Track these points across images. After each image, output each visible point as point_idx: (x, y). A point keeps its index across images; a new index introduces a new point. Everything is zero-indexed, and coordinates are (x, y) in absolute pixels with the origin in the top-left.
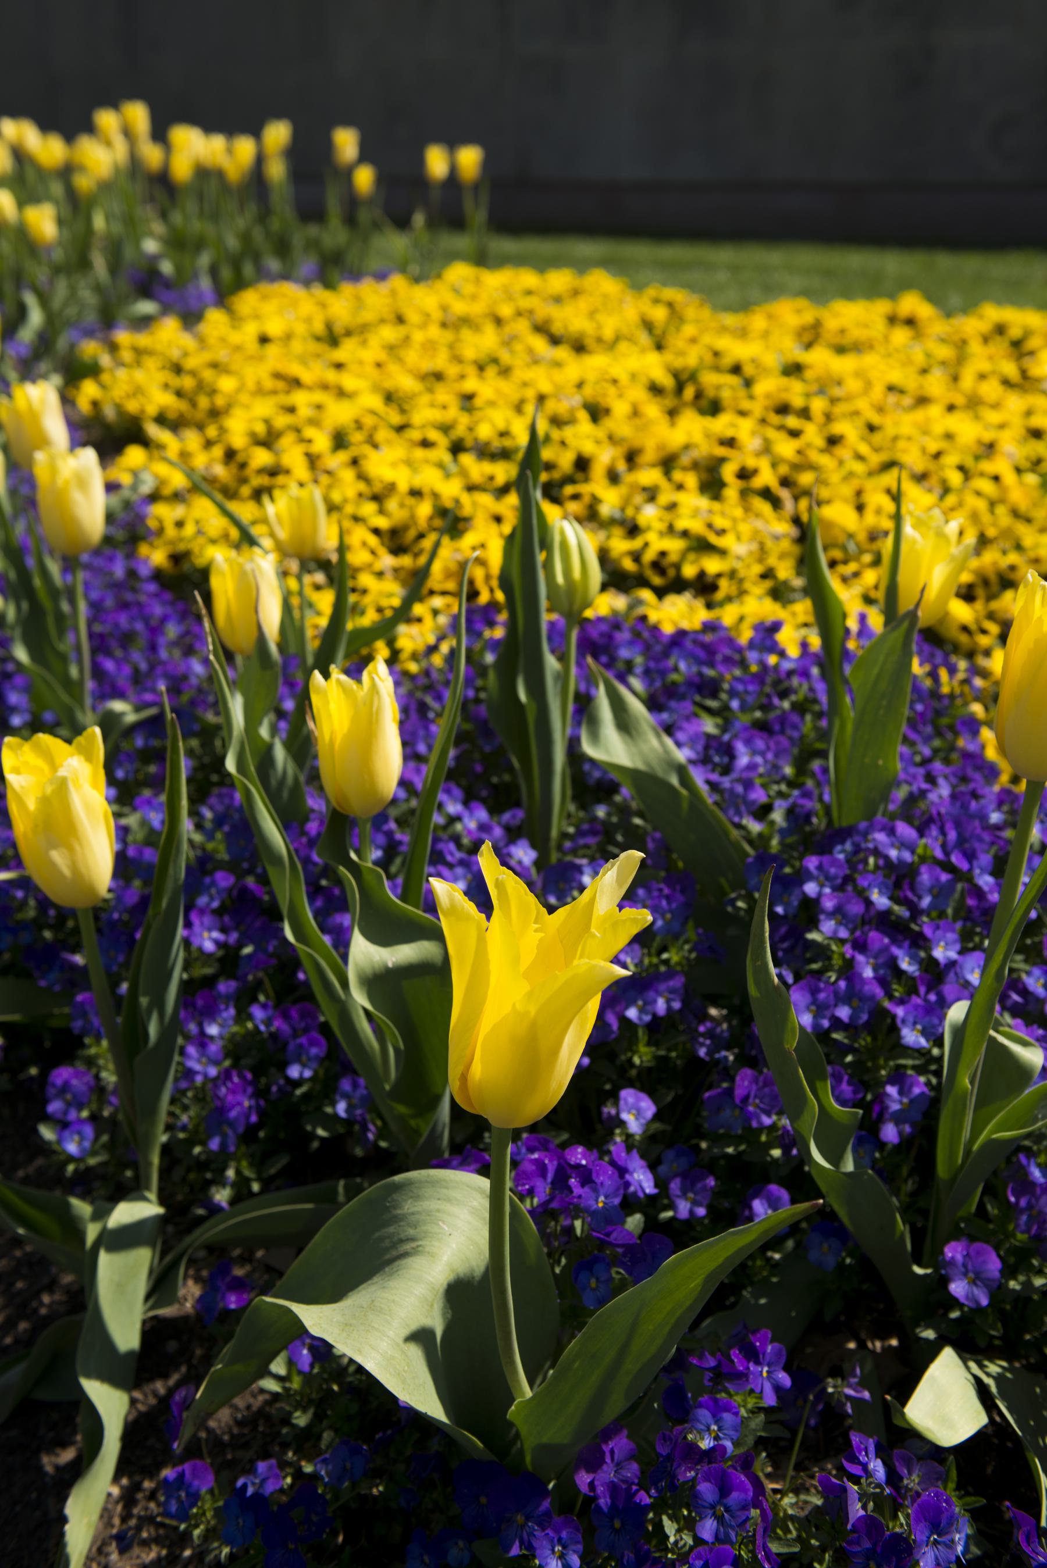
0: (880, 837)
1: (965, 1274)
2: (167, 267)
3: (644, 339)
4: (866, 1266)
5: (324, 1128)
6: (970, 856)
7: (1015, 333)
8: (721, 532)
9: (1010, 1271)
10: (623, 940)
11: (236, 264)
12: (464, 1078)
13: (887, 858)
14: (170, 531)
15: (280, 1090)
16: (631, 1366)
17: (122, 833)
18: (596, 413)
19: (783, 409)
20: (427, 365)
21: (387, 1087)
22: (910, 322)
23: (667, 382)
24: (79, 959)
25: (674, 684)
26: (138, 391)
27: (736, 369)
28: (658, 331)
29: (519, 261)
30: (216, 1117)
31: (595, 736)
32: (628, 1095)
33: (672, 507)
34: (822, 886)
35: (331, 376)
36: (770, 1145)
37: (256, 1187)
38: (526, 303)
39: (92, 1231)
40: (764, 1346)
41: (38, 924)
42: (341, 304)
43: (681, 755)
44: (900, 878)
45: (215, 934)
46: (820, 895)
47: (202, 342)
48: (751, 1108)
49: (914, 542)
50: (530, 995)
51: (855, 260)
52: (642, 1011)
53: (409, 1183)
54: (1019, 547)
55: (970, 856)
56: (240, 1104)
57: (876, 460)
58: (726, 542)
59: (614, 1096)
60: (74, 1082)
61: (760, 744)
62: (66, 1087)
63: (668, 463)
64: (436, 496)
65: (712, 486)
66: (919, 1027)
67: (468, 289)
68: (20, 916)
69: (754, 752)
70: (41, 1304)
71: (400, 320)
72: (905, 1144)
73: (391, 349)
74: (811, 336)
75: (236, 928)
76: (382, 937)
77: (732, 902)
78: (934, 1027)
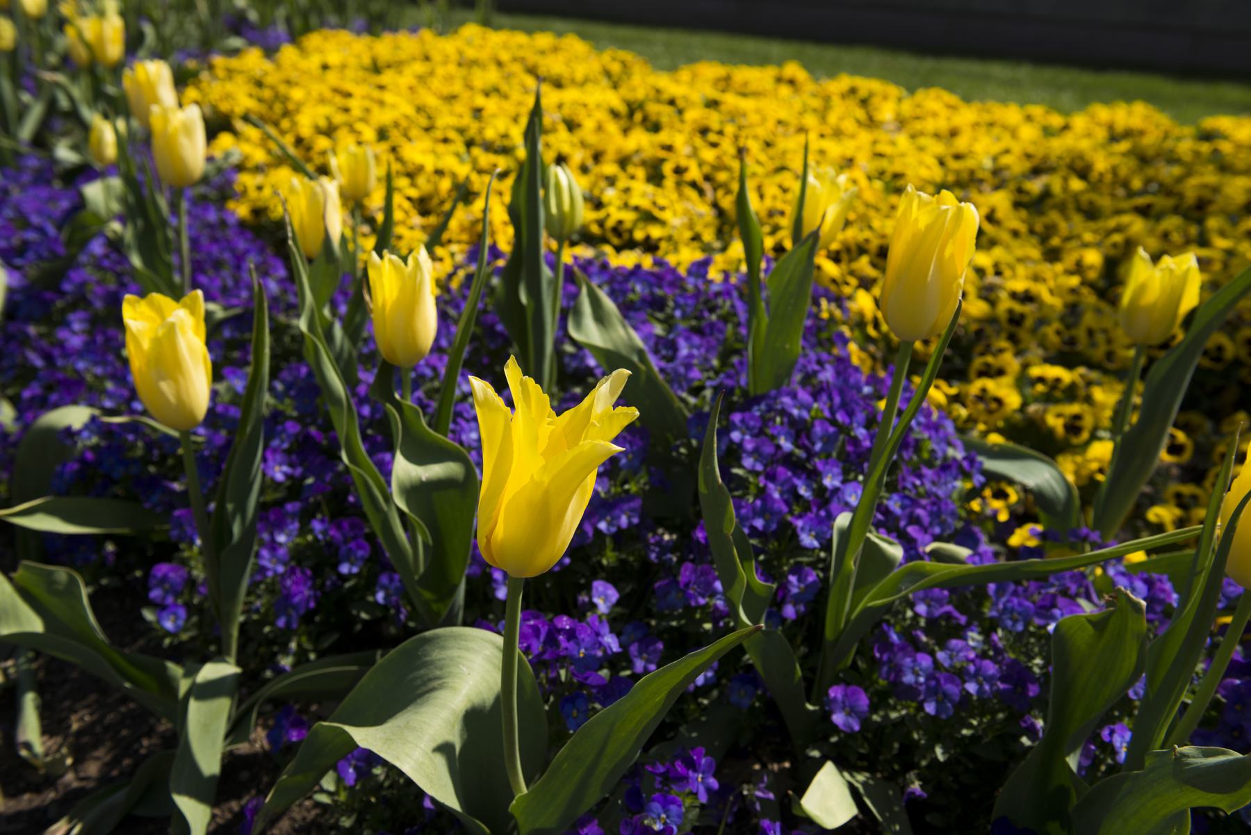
0: (786, 400)
1: (843, 709)
2: (253, 16)
3: (605, 82)
4: (771, 707)
5: (367, 612)
6: (850, 414)
7: (863, 93)
8: (662, 209)
9: (874, 708)
10: (616, 430)
11: (305, 15)
12: (489, 539)
13: (790, 415)
14: (253, 194)
15: (333, 584)
16: (606, 765)
17: (214, 394)
18: (572, 126)
19: (704, 131)
20: (446, 90)
21: (416, 578)
22: (792, 82)
23: (622, 109)
24: (177, 486)
25: (632, 302)
26: (228, 97)
27: (672, 102)
28: (615, 79)
29: (513, 28)
30: (283, 601)
31: (579, 325)
32: (599, 585)
33: (627, 190)
34: (743, 434)
35: (376, 94)
36: (703, 621)
37: (312, 656)
38: (521, 53)
39: (184, 686)
40: (699, 759)
41: (146, 460)
42: (384, 46)
43: (638, 341)
44: (800, 430)
45: (285, 468)
46: (742, 440)
47: (279, 66)
48: (691, 592)
49: (814, 188)
50: (545, 468)
51: (751, 45)
52: (610, 524)
53: (437, 637)
54: (870, 227)
55: (850, 414)
56: (301, 592)
57: (771, 166)
58: (666, 215)
59: (588, 588)
60: (172, 575)
61: (696, 340)
62: (165, 579)
63: (623, 162)
64: (454, 175)
65: (655, 177)
66: (813, 533)
67: (477, 41)
68: (131, 454)
69: (692, 346)
70: (142, 746)
71: (427, 58)
72: (800, 620)
73: (422, 79)
74: (725, 83)
75: (301, 464)
76: (420, 455)
77: (677, 448)
78: (824, 533)
